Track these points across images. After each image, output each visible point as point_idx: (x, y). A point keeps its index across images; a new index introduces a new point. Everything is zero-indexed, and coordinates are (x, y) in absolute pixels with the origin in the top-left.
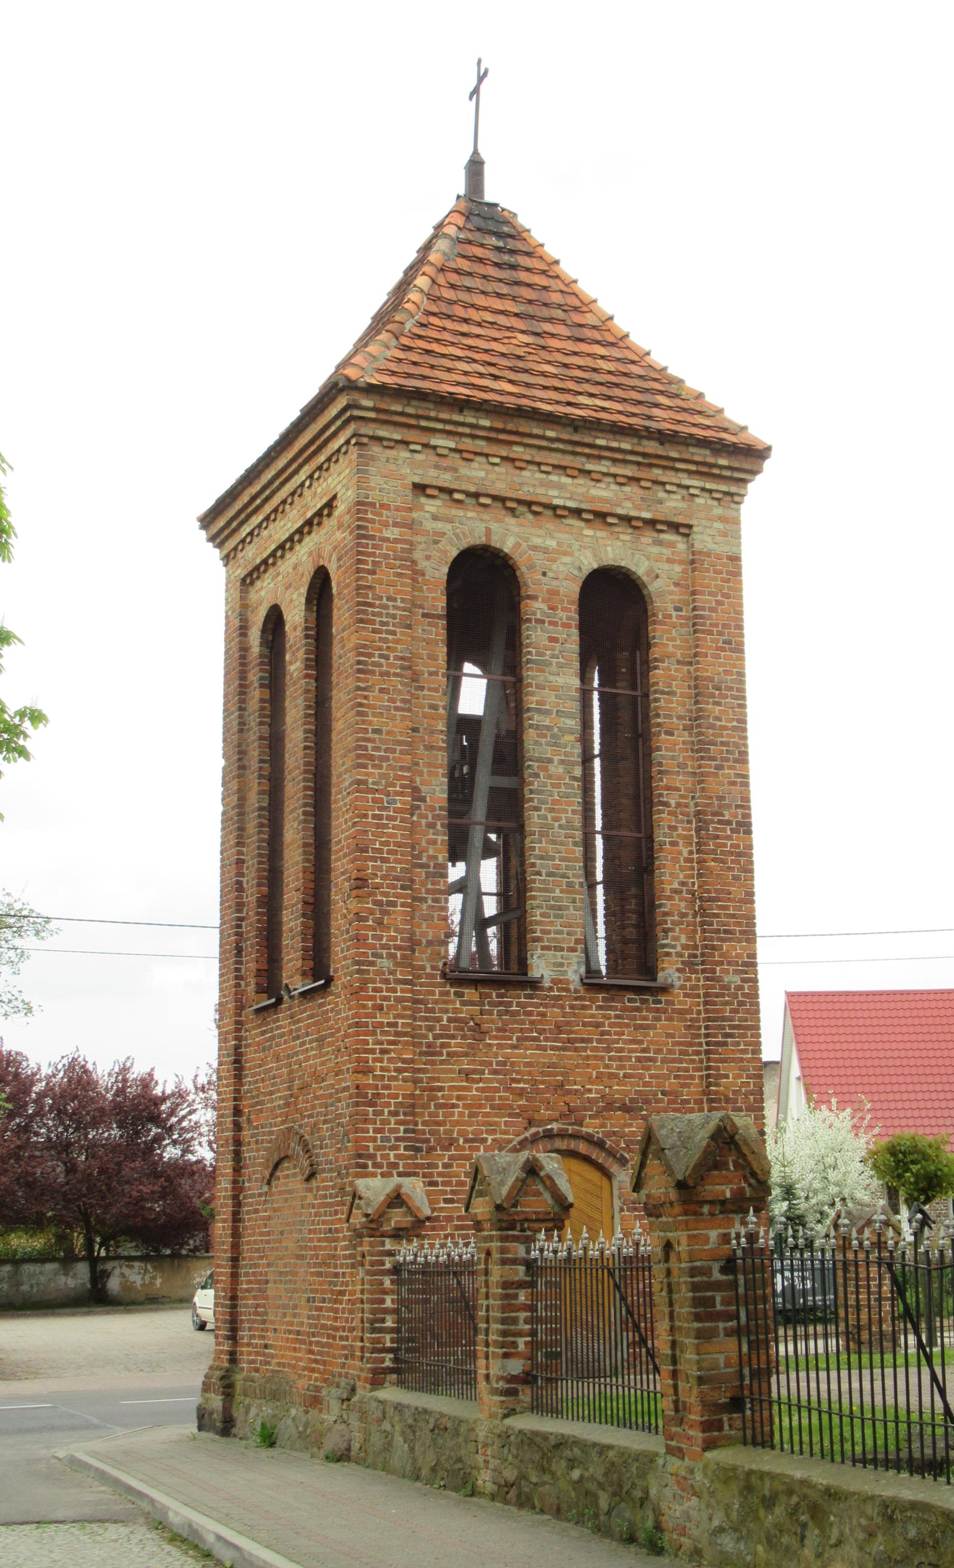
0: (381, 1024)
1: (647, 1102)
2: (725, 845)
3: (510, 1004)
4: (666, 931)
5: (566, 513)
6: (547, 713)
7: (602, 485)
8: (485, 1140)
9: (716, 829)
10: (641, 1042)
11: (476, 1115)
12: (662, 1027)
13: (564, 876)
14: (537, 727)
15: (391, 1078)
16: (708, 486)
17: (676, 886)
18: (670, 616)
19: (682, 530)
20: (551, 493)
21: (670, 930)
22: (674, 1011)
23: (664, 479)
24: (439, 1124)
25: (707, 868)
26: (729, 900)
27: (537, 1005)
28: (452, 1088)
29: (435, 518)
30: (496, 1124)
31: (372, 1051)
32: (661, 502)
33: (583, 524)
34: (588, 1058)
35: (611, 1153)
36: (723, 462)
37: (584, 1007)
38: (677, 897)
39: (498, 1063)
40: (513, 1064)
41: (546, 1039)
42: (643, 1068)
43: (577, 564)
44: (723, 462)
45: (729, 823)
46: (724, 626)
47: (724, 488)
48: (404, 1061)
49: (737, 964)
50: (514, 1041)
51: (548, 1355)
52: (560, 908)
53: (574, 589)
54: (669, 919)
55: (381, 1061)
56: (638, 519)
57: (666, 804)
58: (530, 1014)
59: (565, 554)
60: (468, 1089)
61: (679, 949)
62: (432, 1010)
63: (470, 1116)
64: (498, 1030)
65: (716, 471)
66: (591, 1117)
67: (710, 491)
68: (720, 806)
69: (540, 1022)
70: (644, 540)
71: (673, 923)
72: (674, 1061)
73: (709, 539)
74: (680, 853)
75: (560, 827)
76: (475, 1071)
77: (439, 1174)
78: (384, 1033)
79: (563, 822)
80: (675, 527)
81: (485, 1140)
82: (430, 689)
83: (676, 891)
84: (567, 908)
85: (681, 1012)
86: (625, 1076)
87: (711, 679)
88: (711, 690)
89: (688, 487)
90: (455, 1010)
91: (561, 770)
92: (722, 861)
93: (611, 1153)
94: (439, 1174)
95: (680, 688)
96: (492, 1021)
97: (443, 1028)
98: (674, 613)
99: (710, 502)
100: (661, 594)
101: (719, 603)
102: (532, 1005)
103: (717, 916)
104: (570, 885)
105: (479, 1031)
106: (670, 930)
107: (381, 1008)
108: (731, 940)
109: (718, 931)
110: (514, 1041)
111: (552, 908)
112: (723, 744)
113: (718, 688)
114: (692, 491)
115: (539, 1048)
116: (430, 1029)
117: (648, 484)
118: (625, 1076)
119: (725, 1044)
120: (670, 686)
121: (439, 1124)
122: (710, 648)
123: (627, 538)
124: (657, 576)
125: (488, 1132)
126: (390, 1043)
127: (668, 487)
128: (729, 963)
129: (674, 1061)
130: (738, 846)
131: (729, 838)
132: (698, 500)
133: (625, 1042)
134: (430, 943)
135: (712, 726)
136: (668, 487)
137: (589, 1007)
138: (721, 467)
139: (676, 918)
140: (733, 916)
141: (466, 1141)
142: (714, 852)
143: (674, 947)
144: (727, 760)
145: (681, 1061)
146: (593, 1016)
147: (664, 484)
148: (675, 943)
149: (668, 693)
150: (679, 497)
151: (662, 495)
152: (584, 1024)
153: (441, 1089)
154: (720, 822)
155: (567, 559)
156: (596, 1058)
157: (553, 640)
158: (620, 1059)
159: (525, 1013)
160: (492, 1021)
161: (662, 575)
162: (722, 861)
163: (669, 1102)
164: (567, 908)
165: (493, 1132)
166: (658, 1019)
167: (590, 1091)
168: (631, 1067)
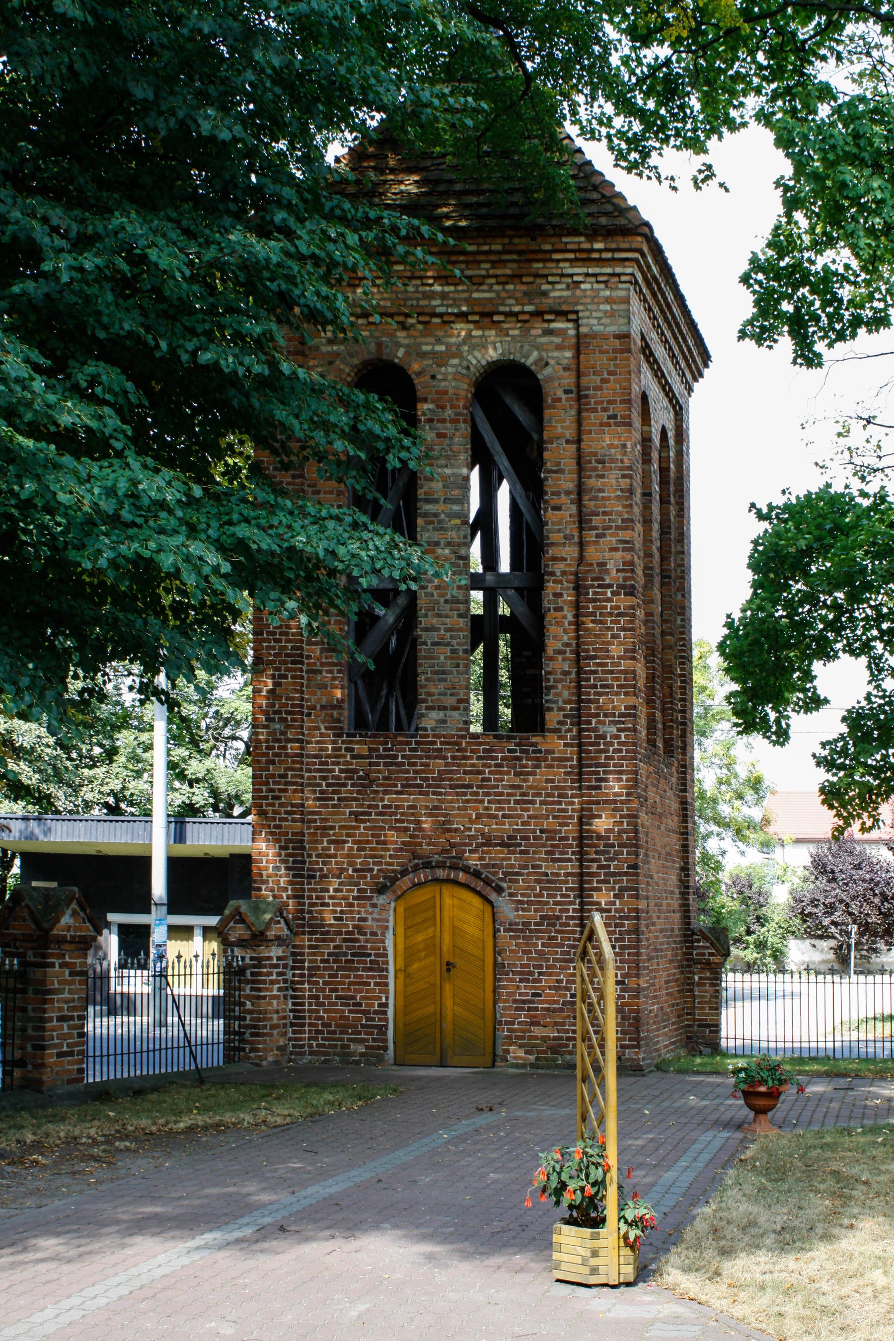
0: (273, 776)
1: (526, 838)
2: (605, 607)
3: (396, 757)
4: (549, 688)
5: (452, 318)
6: (436, 501)
7: (485, 287)
8: (372, 870)
9: (595, 593)
10: (520, 787)
11: (364, 849)
12: (542, 774)
13: (448, 644)
14: (426, 515)
15: (281, 820)
16: (591, 271)
17: (559, 646)
18: (559, 400)
19: (571, 317)
20: (434, 303)
21: (552, 687)
22: (553, 759)
23: (546, 272)
24: (330, 856)
25: (586, 630)
26: (608, 657)
27: (420, 757)
28: (341, 827)
29: (330, 342)
30: (381, 857)
31: (266, 798)
32: (545, 294)
33: (471, 326)
34: (468, 801)
35: (487, 882)
36: (599, 246)
37: (465, 758)
38: (560, 658)
39: (384, 807)
40: (397, 807)
41: (429, 786)
42: (522, 809)
43: (465, 363)
44: (599, 246)
45: (610, 586)
46: (609, 402)
47: (609, 270)
48: (293, 805)
49: (614, 715)
50: (399, 788)
51: (35, 1047)
52: (444, 672)
53: (464, 389)
54: (551, 677)
55: (273, 805)
56: (523, 313)
57: (553, 574)
58: (415, 764)
59: (454, 356)
60: (358, 828)
61: (561, 704)
62: (326, 763)
63: (359, 849)
64: (385, 778)
65: (595, 255)
66: (470, 851)
67: (595, 275)
68: (600, 572)
69: (424, 771)
70: (533, 332)
71: (555, 681)
72: (553, 803)
73: (595, 322)
74: (565, 617)
75: (446, 601)
76: (363, 813)
77: (331, 897)
78: (275, 783)
79: (449, 597)
80: (562, 314)
81: (372, 870)
82: (326, 492)
83: (559, 652)
84: (451, 672)
85: (560, 759)
86: (504, 816)
87: (595, 454)
88: (594, 464)
89: (571, 276)
90: (347, 763)
91: (447, 551)
92: (601, 622)
93: (487, 882)
94: (331, 897)
95: (569, 464)
96: (379, 772)
97: (334, 777)
98: (564, 397)
99: (596, 286)
100: (550, 379)
101: (604, 381)
102: (416, 757)
103: (595, 672)
104: (453, 651)
105: (367, 781)
106: (552, 687)
107: (273, 762)
108: (607, 694)
109: (595, 686)
110: (399, 788)
111: (436, 673)
112: (605, 513)
113: (602, 462)
114: (575, 278)
115: (421, 793)
116: (324, 778)
117: (530, 279)
118: (504, 816)
119: (599, 788)
120: (558, 464)
121: (330, 856)
122: (594, 424)
123: (516, 332)
124: (547, 364)
125: (374, 863)
126: (280, 790)
127: (550, 279)
128: (605, 715)
129: (553, 803)
130: (618, 607)
131: (609, 600)
132: (583, 286)
133: (504, 787)
134: (323, 707)
135: (595, 498)
136: (550, 279)
137: (471, 758)
138: (600, 251)
139: (559, 676)
140: (612, 672)
141: (355, 870)
142: (593, 614)
143: (556, 702)
144: (610, 528)
145: (560, 803)
146: (473, 765)
147: (546, 276)
148: (559, 697)
149: (556, 472)
150: (563, 286)
151: (545, 287)
152: (465, 772)
153: (333, 828)
154: (600, 586)
155: (455, 361)
156: (476, 801)
157: (439, 435)
158: (499, 802)
159: (410, 764)
160: (379, 772)
161: (552, 362)
162: (601, 622)
163: (548, 839)
164: (451, 672)
165: (380, 863)
166: (538, 766)
167: (470, 829)
168: (510, 809)
